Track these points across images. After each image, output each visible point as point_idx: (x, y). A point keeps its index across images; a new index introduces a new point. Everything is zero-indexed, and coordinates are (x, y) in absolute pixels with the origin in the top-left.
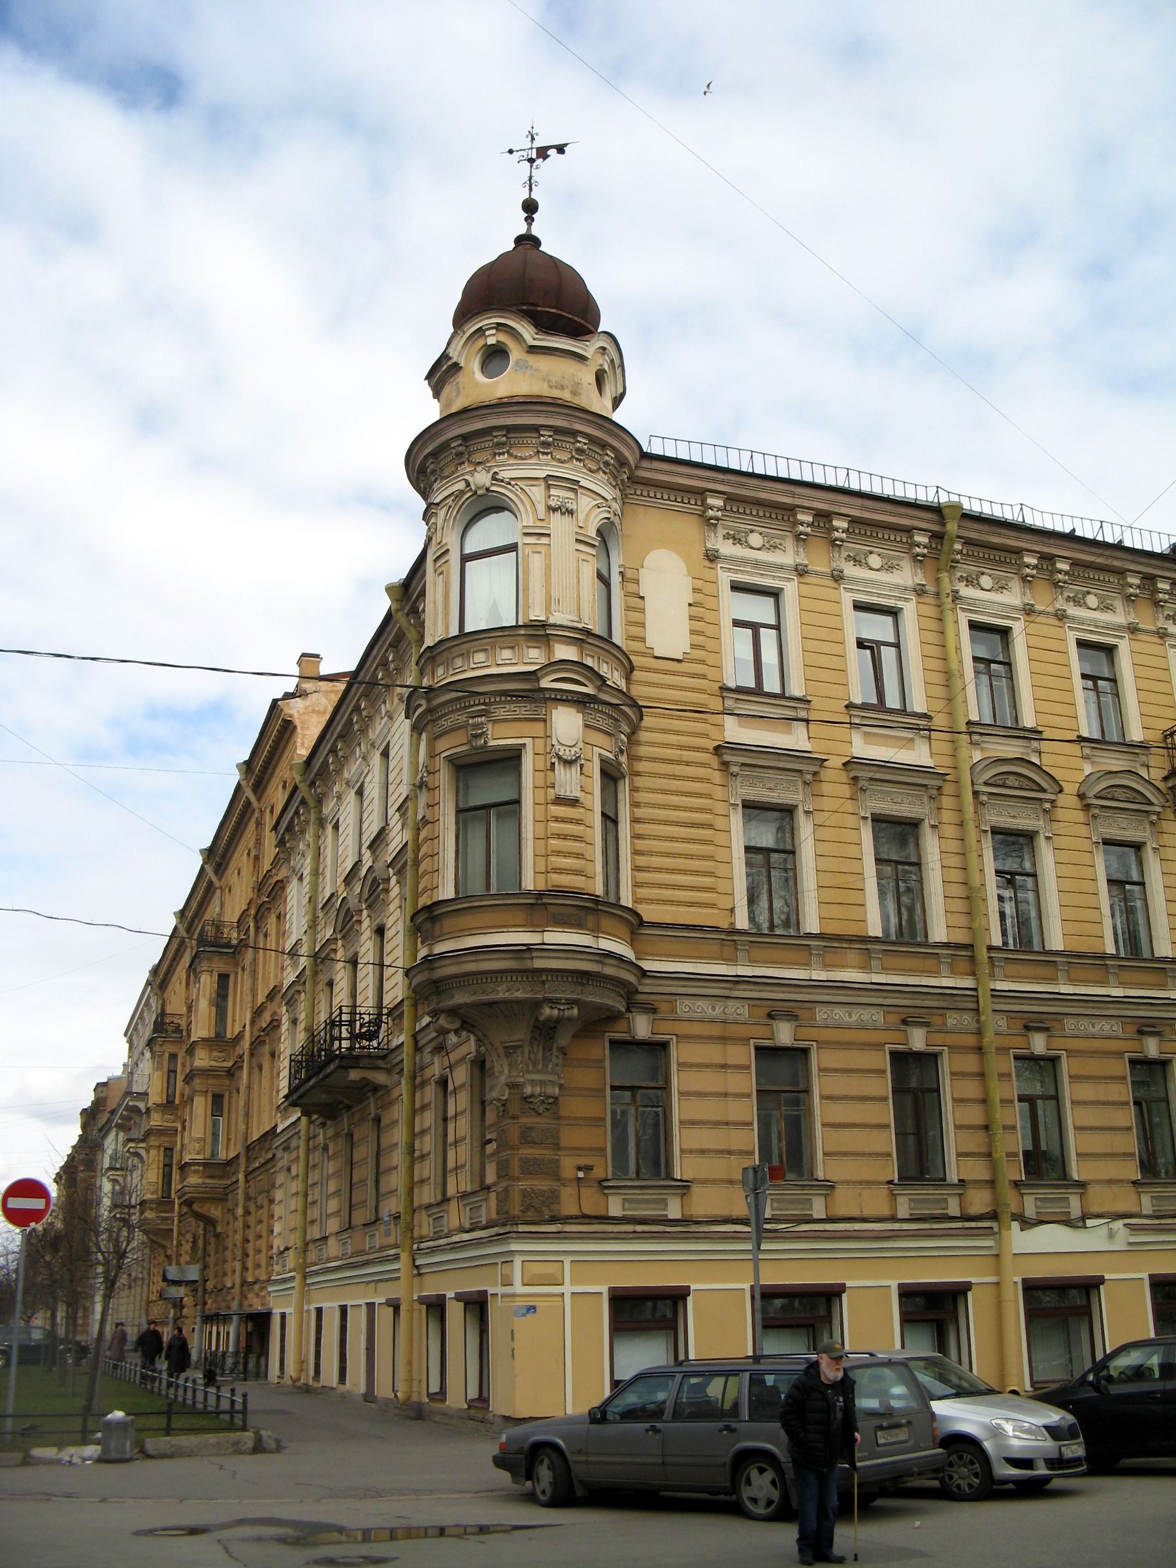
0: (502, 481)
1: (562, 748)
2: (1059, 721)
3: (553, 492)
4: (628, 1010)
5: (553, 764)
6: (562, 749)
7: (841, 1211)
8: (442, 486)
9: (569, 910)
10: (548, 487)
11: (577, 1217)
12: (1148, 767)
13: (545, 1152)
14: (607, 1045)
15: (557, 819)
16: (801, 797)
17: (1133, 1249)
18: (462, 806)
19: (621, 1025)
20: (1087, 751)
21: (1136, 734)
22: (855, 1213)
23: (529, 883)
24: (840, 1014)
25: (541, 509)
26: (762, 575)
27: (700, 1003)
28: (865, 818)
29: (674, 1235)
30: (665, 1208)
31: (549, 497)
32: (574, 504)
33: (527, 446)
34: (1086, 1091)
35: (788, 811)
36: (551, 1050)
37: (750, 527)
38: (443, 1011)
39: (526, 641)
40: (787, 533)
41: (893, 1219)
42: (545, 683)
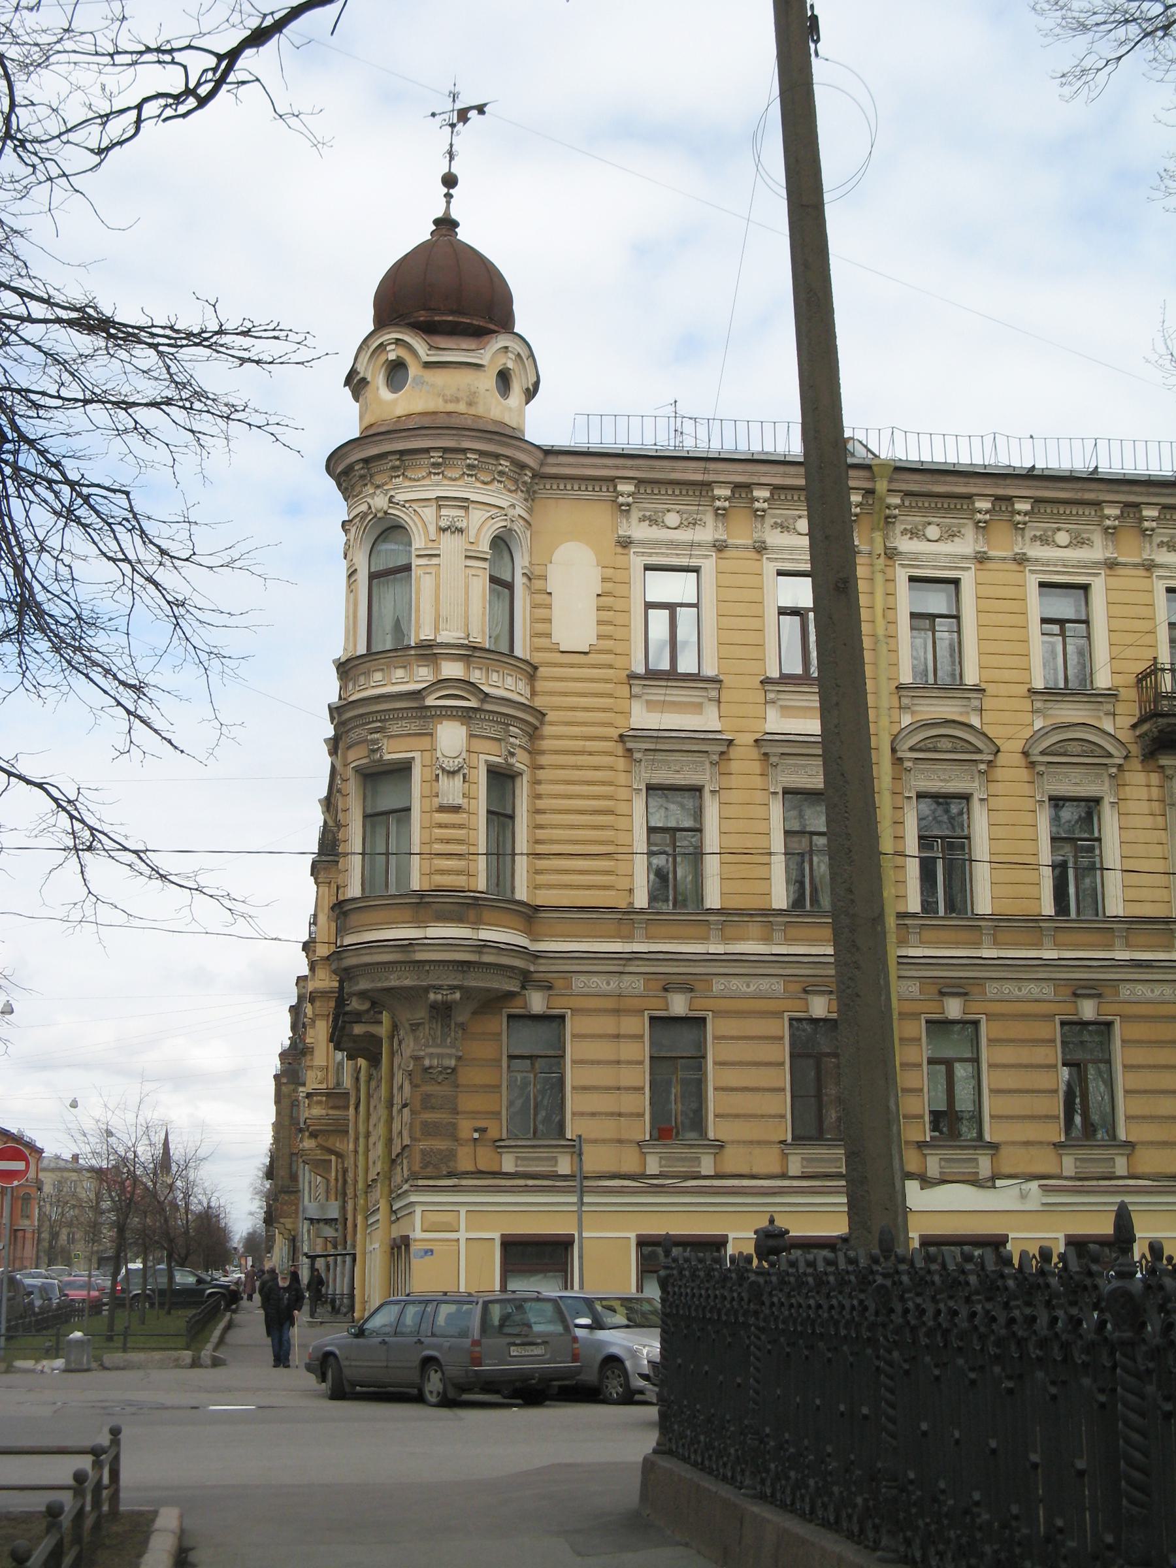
0: (398, 504)
1: (446, 760)
2: (1007, 675)
3: (444, 512)
4: (523, 987)
5: (437, 775)
6: (446, 762)
7: (729, 1168)
8: (356, 502)
9: (456, 908)
10: (439, 507)
11: (472, 1173)
12: (1114, 715)
13: (444, 1116)
14: (505, 1020)
15: (440, 826)
16: (708, 777)
17: (1048, 1210)
18: (369, 811)
19: (518, 1002)
20: (1038, 705)
21: (1103, 680)
22: (744, 1170)
23: (415, 885)
24: (737, 985)
25: (432, 529)
26: (677, 554)
27: (595, 979)
28: (775, 793)
29: (563, 1189)
30: (699, 1165)
31: (440, 517)
32: (465, 521)
33: (420, 467)
34: (1006, 1055)
35: (697, 790)
36: (449, 1026)
37: (667, 506)
38: (355, 994)
39: (417, 660)
40: (707, 508)
41: (784, 1176)
42: (430, 701)
